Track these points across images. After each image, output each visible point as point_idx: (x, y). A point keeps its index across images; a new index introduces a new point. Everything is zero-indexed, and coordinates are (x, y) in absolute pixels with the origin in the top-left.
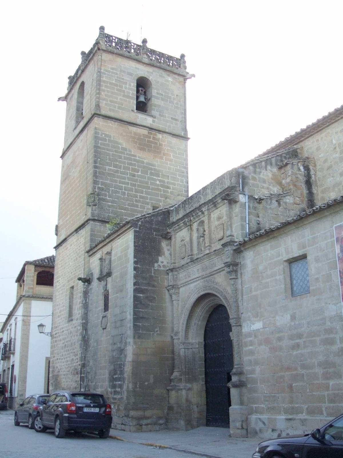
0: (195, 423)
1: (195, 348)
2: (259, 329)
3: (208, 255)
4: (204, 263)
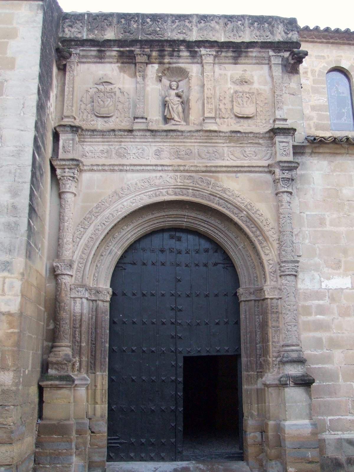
0: (242, 451)
1: (103, 301)
2: (342, 289)
3: (207, 134)
4: (185, 144)
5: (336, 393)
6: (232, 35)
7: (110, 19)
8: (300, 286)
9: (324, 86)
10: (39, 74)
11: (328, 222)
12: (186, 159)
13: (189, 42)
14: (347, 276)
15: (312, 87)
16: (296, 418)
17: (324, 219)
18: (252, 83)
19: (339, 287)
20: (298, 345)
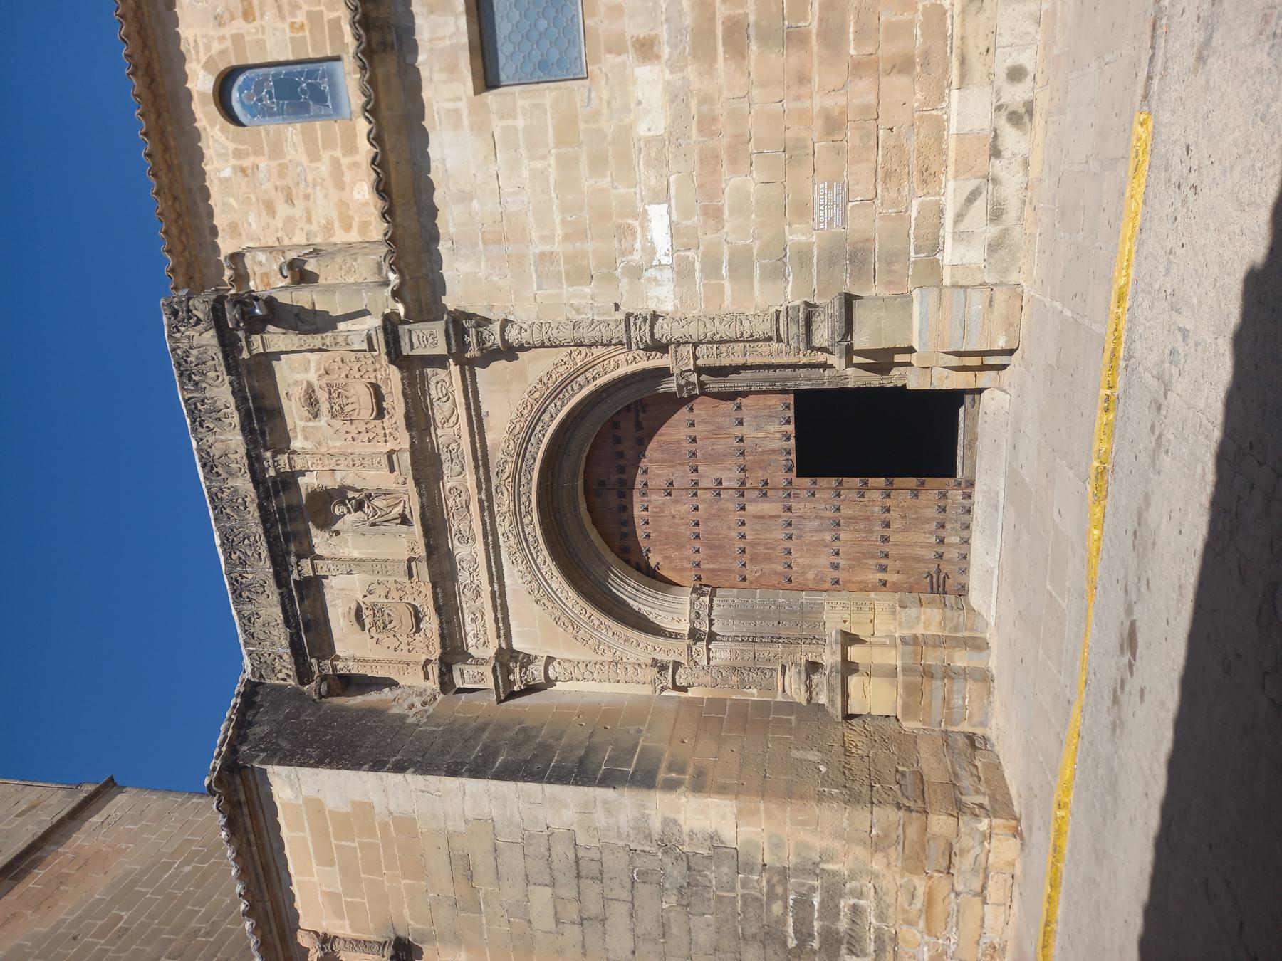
5: (867, 240)
7: (214, 490)
9: (263, 134)
10: (370, 770)
11: (548, 248)
12: (468, 495)
13: (259, 497)
14: (645, 212)
15: (271, 158)
16: (910, 329)
17: (542, 254)
18: (309, 384)
19: (667, 230)
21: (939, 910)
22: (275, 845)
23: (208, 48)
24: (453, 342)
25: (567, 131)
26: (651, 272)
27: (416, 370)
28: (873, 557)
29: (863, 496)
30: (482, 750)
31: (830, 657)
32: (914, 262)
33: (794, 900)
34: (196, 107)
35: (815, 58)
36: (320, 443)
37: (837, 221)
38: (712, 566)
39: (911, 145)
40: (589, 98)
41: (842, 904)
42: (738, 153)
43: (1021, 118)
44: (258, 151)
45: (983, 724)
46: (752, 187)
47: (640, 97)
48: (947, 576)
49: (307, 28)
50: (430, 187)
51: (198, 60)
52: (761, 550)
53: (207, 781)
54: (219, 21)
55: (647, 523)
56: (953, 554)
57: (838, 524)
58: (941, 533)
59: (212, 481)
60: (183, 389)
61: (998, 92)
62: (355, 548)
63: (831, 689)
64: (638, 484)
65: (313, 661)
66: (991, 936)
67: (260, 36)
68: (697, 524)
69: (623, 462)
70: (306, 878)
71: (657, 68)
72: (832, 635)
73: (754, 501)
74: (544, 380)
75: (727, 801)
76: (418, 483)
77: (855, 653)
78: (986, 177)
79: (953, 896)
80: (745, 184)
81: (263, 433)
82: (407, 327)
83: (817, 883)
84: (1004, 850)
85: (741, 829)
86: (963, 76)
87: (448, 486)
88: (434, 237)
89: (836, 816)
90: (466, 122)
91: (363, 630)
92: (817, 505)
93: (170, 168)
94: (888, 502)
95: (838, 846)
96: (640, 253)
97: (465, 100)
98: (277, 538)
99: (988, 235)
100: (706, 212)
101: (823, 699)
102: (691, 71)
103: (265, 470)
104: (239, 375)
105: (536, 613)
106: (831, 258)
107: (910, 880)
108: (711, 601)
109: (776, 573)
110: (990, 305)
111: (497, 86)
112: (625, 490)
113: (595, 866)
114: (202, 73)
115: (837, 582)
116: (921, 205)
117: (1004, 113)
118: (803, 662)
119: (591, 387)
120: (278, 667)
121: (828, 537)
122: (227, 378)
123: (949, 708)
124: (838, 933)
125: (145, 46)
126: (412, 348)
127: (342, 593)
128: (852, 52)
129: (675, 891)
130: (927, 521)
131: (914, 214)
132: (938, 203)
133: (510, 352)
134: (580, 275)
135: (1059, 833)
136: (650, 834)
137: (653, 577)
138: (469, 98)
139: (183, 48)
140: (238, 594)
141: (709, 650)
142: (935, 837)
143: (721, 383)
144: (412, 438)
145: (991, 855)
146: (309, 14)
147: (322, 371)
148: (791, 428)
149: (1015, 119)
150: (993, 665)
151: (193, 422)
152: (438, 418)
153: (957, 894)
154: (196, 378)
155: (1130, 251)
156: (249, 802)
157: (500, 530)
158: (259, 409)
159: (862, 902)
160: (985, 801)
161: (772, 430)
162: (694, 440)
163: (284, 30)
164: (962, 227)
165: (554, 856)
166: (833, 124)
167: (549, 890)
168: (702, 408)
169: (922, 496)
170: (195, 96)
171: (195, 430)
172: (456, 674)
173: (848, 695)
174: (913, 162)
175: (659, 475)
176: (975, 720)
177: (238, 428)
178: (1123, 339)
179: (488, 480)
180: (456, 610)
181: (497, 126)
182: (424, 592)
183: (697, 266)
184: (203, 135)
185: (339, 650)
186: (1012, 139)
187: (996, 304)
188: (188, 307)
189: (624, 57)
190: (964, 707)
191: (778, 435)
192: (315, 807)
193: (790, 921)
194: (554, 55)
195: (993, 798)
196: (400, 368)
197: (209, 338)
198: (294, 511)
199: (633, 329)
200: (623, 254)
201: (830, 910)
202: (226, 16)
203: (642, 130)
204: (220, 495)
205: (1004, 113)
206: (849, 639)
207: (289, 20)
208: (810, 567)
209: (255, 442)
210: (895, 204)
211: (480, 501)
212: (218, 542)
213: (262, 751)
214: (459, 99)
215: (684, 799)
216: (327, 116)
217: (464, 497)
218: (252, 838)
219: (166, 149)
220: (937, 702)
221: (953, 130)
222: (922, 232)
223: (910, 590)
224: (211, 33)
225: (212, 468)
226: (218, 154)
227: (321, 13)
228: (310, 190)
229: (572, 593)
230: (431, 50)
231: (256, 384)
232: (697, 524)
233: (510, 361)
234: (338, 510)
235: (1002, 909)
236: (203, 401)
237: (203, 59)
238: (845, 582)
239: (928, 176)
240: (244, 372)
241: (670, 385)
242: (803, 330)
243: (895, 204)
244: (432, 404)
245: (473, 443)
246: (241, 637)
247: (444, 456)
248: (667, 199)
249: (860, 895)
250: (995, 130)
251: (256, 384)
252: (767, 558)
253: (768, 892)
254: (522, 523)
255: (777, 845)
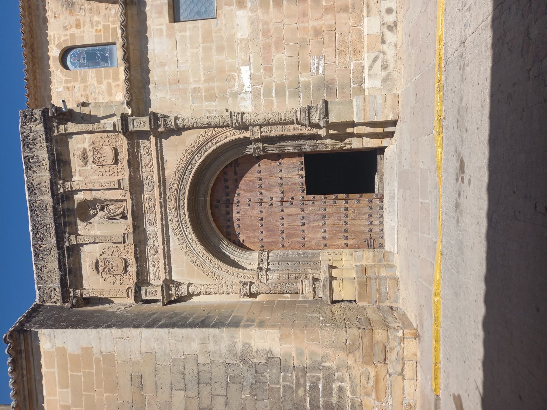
5: (333, 79)
6: (43, 167)
8: (250, 110)
10: (93, 328)
11: (197, 86)
13: (53, 202)
14: (240, 70)
16: (353, 113)
17: (195, 88)
18: (84, 149)
20: (296, 111)
21: (381, 385)
22: (38, 378)
23: (59, 39)
24: (152, 123)
25: (207, 36)
26: (242, 95)
27: (134, 137)
28: (341, 232)
29: (335, 203)
30: (153, 320)
31: (323, 275)
32: (353, 88)
33: (310, 386)
34: (51, 63)
35: (309, 6)
36: (86, 178)
37: (320, 72)
38: (268, 240)
39: (349, 40)
40: (217, 23)
41: (334, 386)
42: (279, 44)
43: (392, 28)
44: (75, 80)
45: (396, 301)
46: (284, 58)
47: (238, 23)
48: (374, 240)
49: (102, 31)
50: (148, 61)
51: (54, 44)
52: (291, 231)
53: (4, 336)
54: (65, 28)
55: (239, 220)
56: (376, 229)
57: (325, 217)
58: (371, 219)
59: (31, 197)
60: (24, 152)
61: (383, 18)
62: (98, 230)
63: (325, 288)
64: (235, 201)
65: (71, 290)
66: (409, 399)
67: (82, 34)
68: (262, 219)
69: (228, 191)
70: (52, 398)
71: (245, 11)
72: (324, 266)
73: (287, 207)
74: (193, 144)
75: (275, 331)
76: (131, 194)
77: (334, 272)
78: (380, 51)
79: (388, 376)
80: (281, 57)
81: (60, 172)
82: (132, 118)
83: (321, 375)
84: (411, 347)
85: (282, 346)
86: (368, 12)
87: (145, 197)
88: (147, 82)
89: (328, 334)
90: (165, 34)
91: (98, 273)
92: (316, 208)
93: (35, 86)
94: (347, 205)
95: (330, 351)
96: (237, 87)
97: (165, 24)
98: (60, 224)
99: (383, 75)
100: (265, 69)
101: (321, 295)
102: (260, 12)
103: (58, 189)
104: (51, 143)
105: (185, 261)
106: (318, 88)
107: (366, 369)
108: (268, 254)
109: (298, 242)
110: (385, 101)
111: (179, 21)
112: (229, 204)
113: (208, 375)
114: (55, 49)
115: (326, 246)
116: (354, 64)
117: (385, 26)
118: (311, 278)
119: (215, 147)
120: (53, 295)
121: (321, 223)
122: (46, 144)
123: (380, 294)
124: (332, 405)
125: (32, 37)
126: (134, 128)
127: (90, 254)
128: (324, 4)
129: (249, 387)
130: (364, 214)
131: (352, 68)
132: (361, 63)
133: (178, 130)
134: (211, 97)
135: (437, 310)
136: (236, 354)
137: (241, 246)
138: (166, 24)
139: (48, 39)
140: (37, 255)
141: (267, 275)
142: (377, 343)
143: (273, 147)
144: (130, 172)
145: (405, 350)
146: (104, 26)
147: (91, 142)
148: (303, 173)
149: (390, 28)
150: (398, 274)
151: (27, 168)
152: (144, 164)
153: (390, 375)
154: (31, 147)
155: (442, 20)
156: (26, 351)
157: (169, 218)
158: (59, 160)
159: (343, 384)
160: (400, 325)
161: (294, 172)
162: (261, 179)
163: (92, 32)
164: (371, 72)
165: (186, 371)
166: (318, 32)
167: (183, 393)
168: (265, 164)
169: (362, 202)
170: (51, 58)
171: (27, 172)
172: (143, 292)
173: (333, 291)
174: (350, 47)
175: (245, 196)
176: (392, 299)
177: (48, 169)
178: (443, 58)
179: (165, 193)
180: (146, 260)
181: (178, 35)
182: (130, 251)
183: (262, 92)
184: (52, 74)
185: (85, 286)
186: (389, 36)
187: (387, 100)
188: (32, 113)
189: (232, 7)
190: (386, 293)
191: (298, 176)
192: (62, 351)
193: (308, 399)
194: (203, 9)
195: (403, 323)
196: (127, 138)
197: (40, 127)
198: (70, 211)
199: (233, 117)
200: (230, 87)
201: (328, 391)
202: (69, 27)
203: (239, 36)
204: (34, 204)
205: (385, 26)
206: (331, 267)
207: (95, 28)
208: (313, 239)
209: (55, 176)
210: (344, 64)
211: (161, 203)
212: (30, 228)
213: (37, 325)
214: (162, 24)
215: (254, 331)
216: (108, 67)
217: (153, 202)
218: (25, 372)
219: (35, 79)
220: (374, 291)
221: (366, 33)
222: (355, 75)
223: (359, 247)
224: (61, 33)
225: (33, 191)
226: (58, 82)
227: (109, 25)
228: (97, 96)
229: (202, 249)
230: (152, 5)
231: (59, 148)
232: (262, 219)
233: (178, 136)
234: (92, 212)
235: (413, 381)
236: (33, 157)
237: (57, 43)
238: (330, 245)
239: (357, 53)
240: (54, 142)
241: (250, 150)
242: (307, 115)
243: (344, 64)
244: (141, 157)
245: (159, 174)
246: (36, 279)
247: (145, 182)
248: (249, 64)
249: (342, 380)
250: (382, 33)
251: (59, 148)
252: (294, 235)
253: (296, 382)
254: (180, 214)
255: (300, 354)
